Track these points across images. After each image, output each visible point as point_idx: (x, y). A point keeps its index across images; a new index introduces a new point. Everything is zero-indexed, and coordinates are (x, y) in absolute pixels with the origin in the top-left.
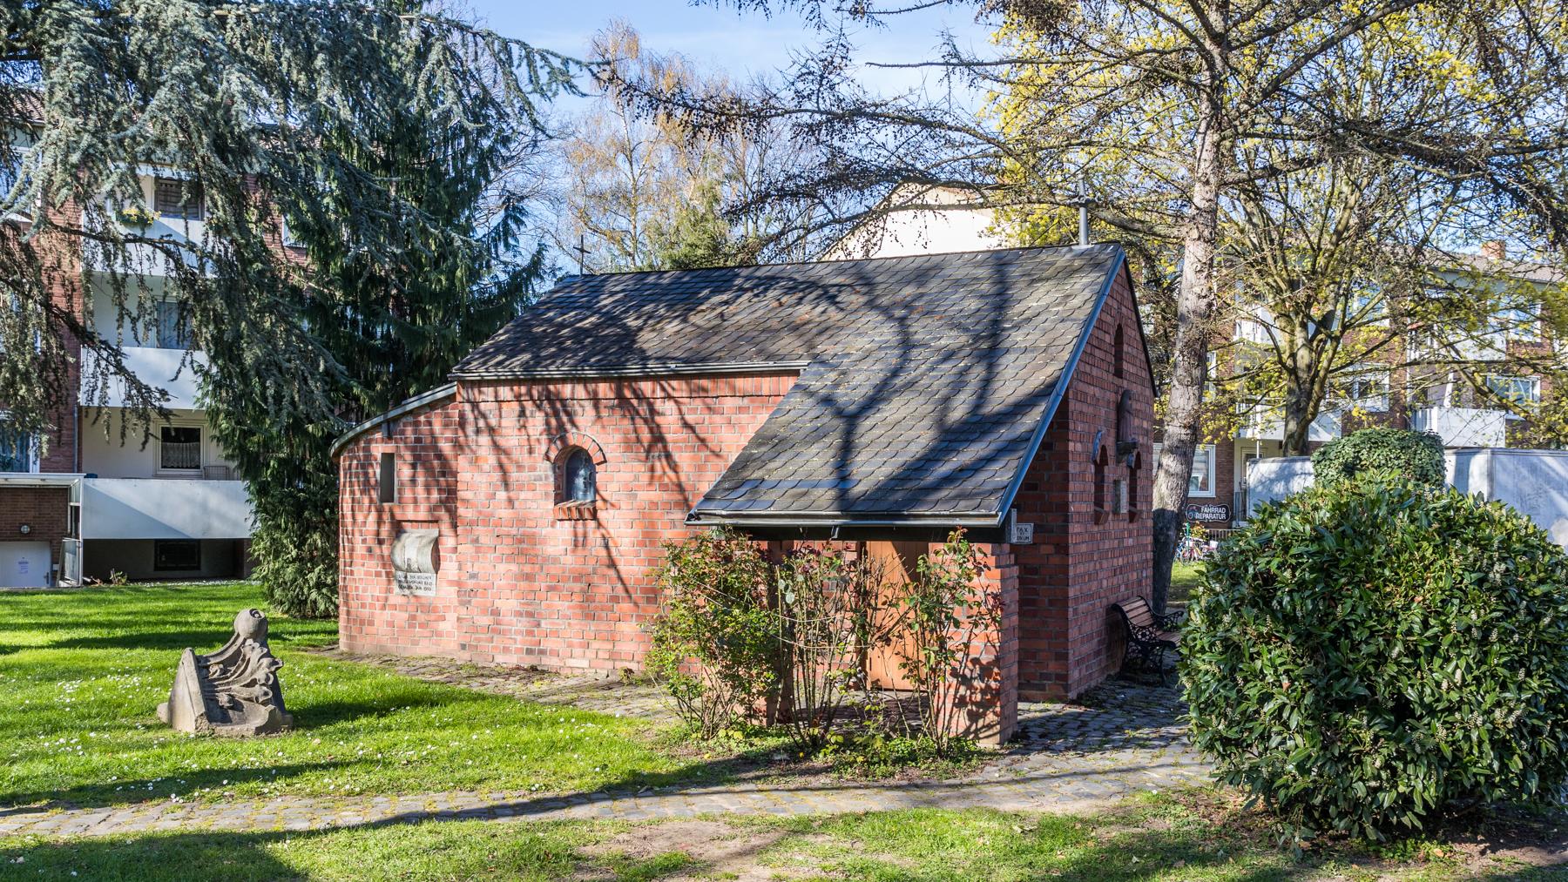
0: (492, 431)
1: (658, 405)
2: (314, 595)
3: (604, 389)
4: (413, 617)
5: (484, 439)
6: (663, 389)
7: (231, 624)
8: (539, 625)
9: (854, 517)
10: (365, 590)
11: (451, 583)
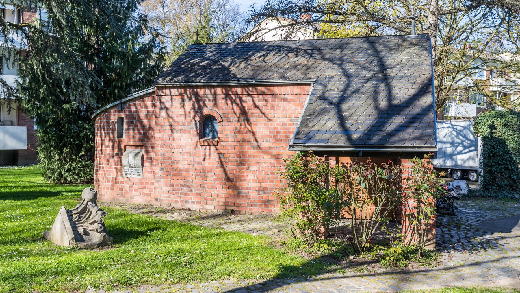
0: (167, 109)
1: (244, 98)
2: (66, 174)
3: (219, 91)
4: (132, 187)
5: (163, 112)
6: (246, 91)
7: (81, 195)
8: (191, 191)
9: (356, 147)
10: (109, 175)
11: (149, 172)
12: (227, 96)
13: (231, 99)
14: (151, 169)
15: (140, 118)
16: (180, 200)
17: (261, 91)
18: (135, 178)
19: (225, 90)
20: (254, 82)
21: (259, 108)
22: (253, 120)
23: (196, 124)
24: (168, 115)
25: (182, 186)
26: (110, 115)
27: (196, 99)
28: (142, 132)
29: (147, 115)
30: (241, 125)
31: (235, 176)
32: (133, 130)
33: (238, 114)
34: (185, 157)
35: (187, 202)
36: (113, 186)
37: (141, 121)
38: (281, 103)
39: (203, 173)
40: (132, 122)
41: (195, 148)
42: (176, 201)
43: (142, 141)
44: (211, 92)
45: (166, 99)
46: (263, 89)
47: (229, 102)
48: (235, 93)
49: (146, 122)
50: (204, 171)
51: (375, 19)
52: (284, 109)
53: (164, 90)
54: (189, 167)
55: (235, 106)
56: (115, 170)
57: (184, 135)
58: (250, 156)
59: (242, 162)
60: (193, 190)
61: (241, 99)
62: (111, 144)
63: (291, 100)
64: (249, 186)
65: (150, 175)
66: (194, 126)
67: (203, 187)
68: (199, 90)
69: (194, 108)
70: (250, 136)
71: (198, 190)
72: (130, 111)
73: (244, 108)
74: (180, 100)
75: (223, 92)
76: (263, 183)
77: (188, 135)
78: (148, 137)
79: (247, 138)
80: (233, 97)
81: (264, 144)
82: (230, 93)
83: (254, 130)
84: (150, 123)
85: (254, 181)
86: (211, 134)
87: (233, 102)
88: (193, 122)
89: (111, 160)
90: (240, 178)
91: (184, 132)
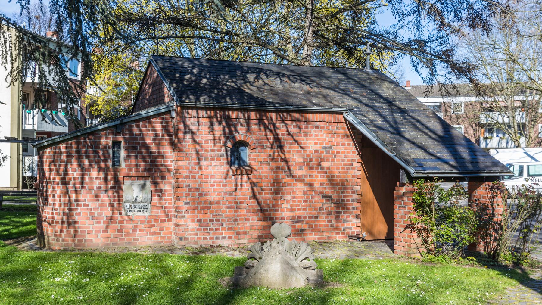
0: (193, 133)
3: (253, 115)
5: (188, 137)
8: (222, 225)
12: (260, 122)
13: (265, 125)
14: (160, 203)
15: (145, 143)
16: (209, 237)
17: (295, 117)
18: (140, 216)
19: (259, 115)
20: (291, 108)
21: (292, 135)
22: (287, 147)
23: (226, 151)
24: (194, 141)
25: (211, 220)
26: (100, 138)
27: (227, 123)
28: (148, 159)
29: (154, 139)
30: (274, 153)
31: (269, 206)
32: (136, 157)
33: (271, 141)
34: (215, 188)
35: (217, 238)
36: (107, 227)
37: (147, 147)
38: (313, 131)
39: (237, 204)
40: (135, 148)
41: (226, 178)
42: (205, 238)
43: (149, 170)
44: (244, 116)
45: (191, 121)
46: (297, 115)
47: (262, 128)
48: (270, 118)
49: (153, 148)
50: (236, 203)
51: (261, 43)
52: (316, 136)
53: (190, 111)
54: (219, 198)
55: (268, 133)
56: (109, 208)
57: (214, 163)
58: (284, 185)
59: (278, 191)
60: (224, 224)
61: (274, 125)
62: (102, 175)
63: (322, 128)
64: (283, 216)
65: (160, 210)
66: (225, 153)
67: (236, 220)
68: (231, 112)
69: (224, 133)
70: (283, 164)
71: (230, 224)
72: (131, 134)
73: (277, 134)
74: (209, 124)
75: (257, 117)
76: (297, 212)
77: (218, 163)
78: (157, 166)
79: (282, 166)
80: (267, 122)
81: (298, 172)
82: (265, 118)
83: (287, 157)
84: (158, 148)
85: (288, 210)
86: (237, 162)
87: (266, 128)
88: (223, 148)
89: (103, 194)
90: (275, 208)
91: (213, 160)
